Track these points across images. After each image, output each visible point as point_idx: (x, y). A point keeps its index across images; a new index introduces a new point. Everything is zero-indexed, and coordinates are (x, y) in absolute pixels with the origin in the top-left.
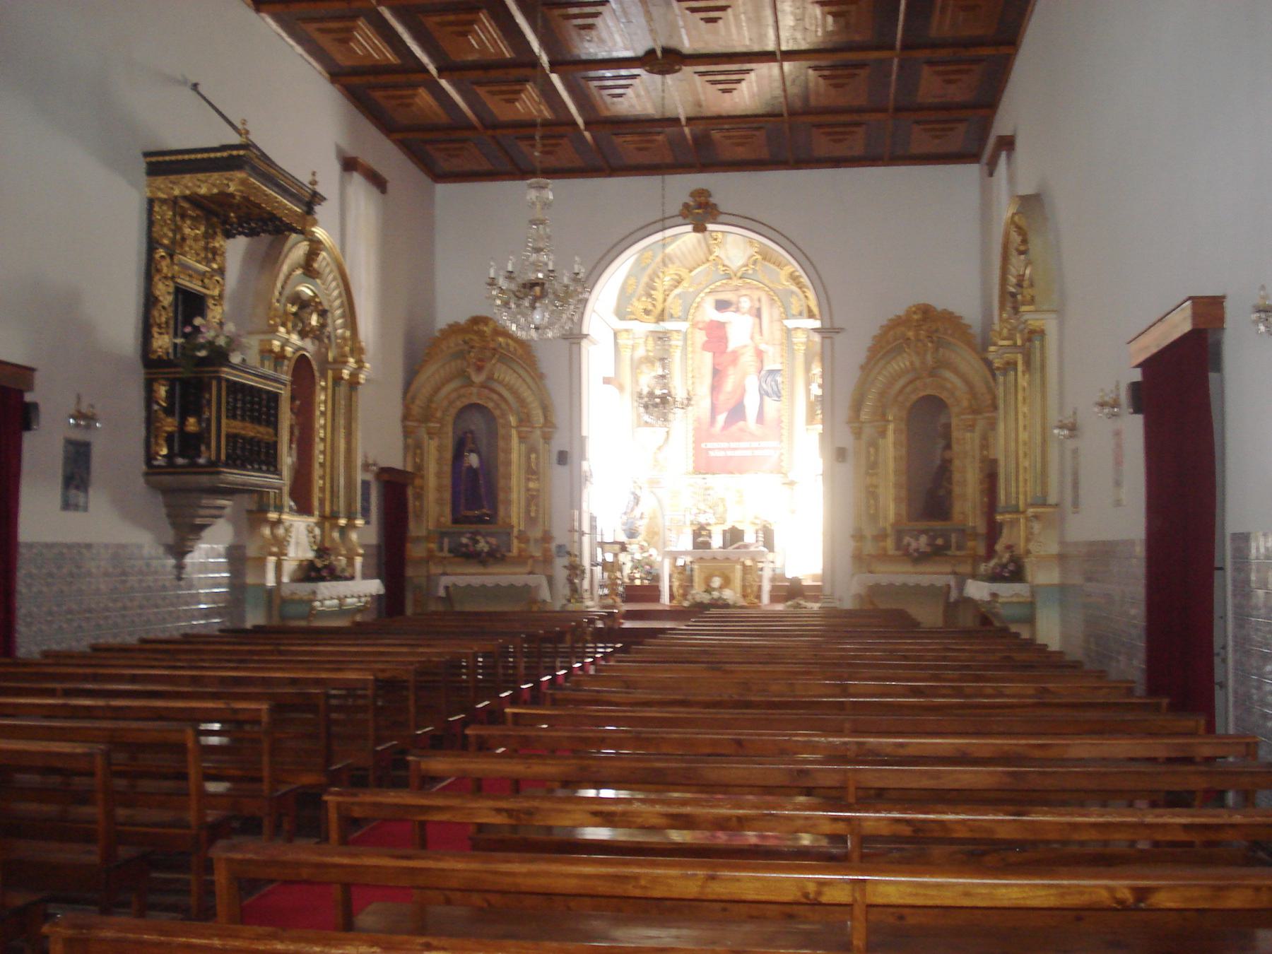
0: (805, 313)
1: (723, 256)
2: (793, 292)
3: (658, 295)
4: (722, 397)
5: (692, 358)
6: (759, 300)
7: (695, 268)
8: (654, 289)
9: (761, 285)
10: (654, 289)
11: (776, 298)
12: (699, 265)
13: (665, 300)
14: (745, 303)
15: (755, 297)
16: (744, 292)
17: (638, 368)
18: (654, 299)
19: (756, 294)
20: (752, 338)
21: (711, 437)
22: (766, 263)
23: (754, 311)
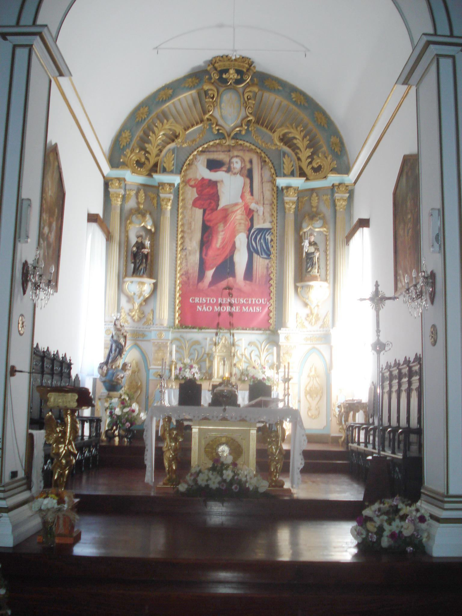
0: (297, 172)
1: (217, 113)
2: (284, 154)
3: (153, 149)
4: (211, 253)
6: (251, 162)
7: (188, 128)
8: (149, 142)
9: (254, 147)
10: (149, 142)
11: (267, 160)
12: (193, 126)
13: (158, 155)
14: (237, 165)
15: (247, 159)
16: (236, 153)
17: (127, 218)
18: (148, 152)
19: (247, 156)
20: (242, 197)
21: (198, 292)
22: (259, 127)
23: (245, 172)
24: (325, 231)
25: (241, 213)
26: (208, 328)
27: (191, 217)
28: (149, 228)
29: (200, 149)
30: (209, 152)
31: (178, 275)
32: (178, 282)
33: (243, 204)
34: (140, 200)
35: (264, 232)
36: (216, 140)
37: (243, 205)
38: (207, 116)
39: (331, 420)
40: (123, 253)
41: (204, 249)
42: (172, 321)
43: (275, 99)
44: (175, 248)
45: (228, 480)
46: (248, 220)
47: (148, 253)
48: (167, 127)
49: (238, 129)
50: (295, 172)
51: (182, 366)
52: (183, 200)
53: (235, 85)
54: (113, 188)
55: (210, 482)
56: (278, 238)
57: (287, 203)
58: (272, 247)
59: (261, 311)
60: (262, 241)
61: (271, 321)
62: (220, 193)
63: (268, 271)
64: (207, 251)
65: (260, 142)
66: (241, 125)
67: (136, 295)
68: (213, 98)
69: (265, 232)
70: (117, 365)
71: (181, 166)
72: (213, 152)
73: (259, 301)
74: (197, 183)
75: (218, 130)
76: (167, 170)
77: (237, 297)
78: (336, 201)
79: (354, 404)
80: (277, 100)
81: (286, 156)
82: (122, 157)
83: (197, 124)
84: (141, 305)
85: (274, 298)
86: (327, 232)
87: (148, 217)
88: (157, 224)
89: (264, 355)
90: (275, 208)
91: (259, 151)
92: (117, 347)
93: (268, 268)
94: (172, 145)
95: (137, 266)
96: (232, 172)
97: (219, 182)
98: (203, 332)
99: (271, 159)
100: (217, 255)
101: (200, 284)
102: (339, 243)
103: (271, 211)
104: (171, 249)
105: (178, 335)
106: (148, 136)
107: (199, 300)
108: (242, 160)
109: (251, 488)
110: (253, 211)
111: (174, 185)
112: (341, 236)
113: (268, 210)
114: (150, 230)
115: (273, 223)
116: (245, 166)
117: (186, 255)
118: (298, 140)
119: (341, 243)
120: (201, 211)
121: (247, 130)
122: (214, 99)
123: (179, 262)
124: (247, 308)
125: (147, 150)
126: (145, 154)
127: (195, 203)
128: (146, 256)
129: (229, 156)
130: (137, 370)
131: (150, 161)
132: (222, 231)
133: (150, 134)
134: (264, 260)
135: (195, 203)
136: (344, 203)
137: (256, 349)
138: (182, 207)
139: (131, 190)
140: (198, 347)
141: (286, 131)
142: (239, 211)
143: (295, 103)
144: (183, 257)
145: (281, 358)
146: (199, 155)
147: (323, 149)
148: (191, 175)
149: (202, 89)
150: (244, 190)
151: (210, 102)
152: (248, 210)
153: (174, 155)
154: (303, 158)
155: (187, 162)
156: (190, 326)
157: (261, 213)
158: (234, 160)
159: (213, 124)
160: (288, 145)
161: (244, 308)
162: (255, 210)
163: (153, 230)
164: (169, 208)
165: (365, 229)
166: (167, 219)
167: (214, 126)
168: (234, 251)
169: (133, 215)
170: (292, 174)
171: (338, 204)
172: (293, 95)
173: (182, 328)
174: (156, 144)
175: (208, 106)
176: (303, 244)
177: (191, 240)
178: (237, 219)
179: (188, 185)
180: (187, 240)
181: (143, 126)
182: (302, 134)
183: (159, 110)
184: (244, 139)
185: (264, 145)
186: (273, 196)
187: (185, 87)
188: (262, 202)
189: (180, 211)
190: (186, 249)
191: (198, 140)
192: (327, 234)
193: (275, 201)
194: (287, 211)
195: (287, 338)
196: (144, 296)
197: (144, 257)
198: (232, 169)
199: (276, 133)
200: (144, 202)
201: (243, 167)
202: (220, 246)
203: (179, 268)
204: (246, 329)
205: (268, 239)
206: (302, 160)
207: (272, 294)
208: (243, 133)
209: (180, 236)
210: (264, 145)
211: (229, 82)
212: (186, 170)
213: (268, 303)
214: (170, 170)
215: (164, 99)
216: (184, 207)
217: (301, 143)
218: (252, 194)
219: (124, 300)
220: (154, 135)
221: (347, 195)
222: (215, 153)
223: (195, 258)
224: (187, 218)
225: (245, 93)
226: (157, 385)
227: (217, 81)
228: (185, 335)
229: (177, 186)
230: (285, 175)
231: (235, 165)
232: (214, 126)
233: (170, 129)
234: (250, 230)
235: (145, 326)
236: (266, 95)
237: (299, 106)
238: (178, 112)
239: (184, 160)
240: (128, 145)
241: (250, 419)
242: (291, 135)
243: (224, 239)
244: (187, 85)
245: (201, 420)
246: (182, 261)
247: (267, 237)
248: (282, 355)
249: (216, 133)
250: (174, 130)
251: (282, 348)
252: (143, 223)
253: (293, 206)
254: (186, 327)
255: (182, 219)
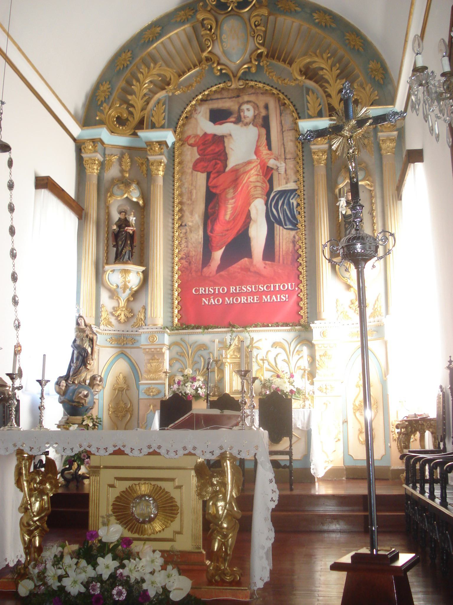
0: (326, 111)
1: (218, 51)
2: (308, 90)
3: (137, 102)
4: (218, 228)
5: (180, 179)
6: (266, 107)
7: (184, 73)
8: (132, 93)
9: (268, 88)
10: (132, 93)
11: (287, 101)
12: (189, 69)
13: (143, 109)
14: (249, 112)
15: (261, 104)
16: (246, 98)
17: (108, 191)
18: (133, 106)
19: (261, 101)
20: (257, 152)
21: (203, 280)
22: (274, 62)
23: (260, 121)
24: (368, 185)
25: (256, 173)
26: (217, 328)
27: (192, 185)
28: (135, 200)
29: (200, 97)
30: (212, 100)
31: (176, 259)
32: (176, 268)
33: (259, 161)
34: (123, 167)
35: (287, 194)
36: (220, 84)
37: (258, 162)
38: (205, 54)
39: (390, 447)
40: (103, 235)
41: (209, 223)
42: (170, 319)
43: (292, 24)
44: (171, 225)
45: (105, 577)
46: (266, 181)
47: (134, 232)
48: (155, 72)
49: (246, 66)
50: (323, 112)
51: (181, 378)
52: (179, 163)
53: (237, 10)
54: (86, 153)
55: (67, 582)
56: (306, 201)
57: (314, 153)
58: (299, 213)
59: (287, 300)
60: (285, 207)
61: (302, 313)
62: (228, 151)
63: (295, 246)
64: (213, 226)
65: (275, 78)
66: (249, 60)
67: (120, 287)
68: (210, 30)
69: (289, 194)
70: (82, 380)
71: (176, 120)
72: (218, 99)
73: (284, 286)
74: (198, 140)
75: (221, 70)
76: (156, 125)
77: (255, 283)
78: (381, 142)
79: (417, 421)
80: (295, 24)
81: (310, 93)
82: (99, 113)
83: (195, 66)
84: (128, 301)
85: (304, 282)
86: (371, 186)
87: (134, 186)
88: (146, 196)
89: (294, 359)
90: (301, 162)
91: (275, 91)
92: (79, 353)
93: (294, 242)
94: (161, 95)
95: (120, 249)
96: (243, 122)
97: (226, 136)
98: (210, 333)
99: (292, 100)
100: (228, 230)
101: (205, 269)
102: (388, 200)
103: (295, 167)
104: (165, 226)
105: (177, 338)
106: (131, 85)
107: (205, 291)
108: (256, 106)
109: (152, 593)
110: (272, 169)
111: (165, 143)
112: (390, 189)
113: (292, 166)
114: (137, 203)
115: (299, 183)
116: (259, 114)
117: (186, 233)
118: (324, 71)
119: (391, 199)
120: (204, 175)
121: (258, 67)
122: (213, 31)
123: (176, 242)
124: (269, 297)
125: (131, 102)
126: (127, 108)
127: (196, 167)
128: (132, 237)
129: (238, 102)
130: (125, 387)
131: (135, 116)
132: (232, 198)
133: (132, 82)
134: (288, 231)
135: (196, 167)
136: (392, 145)
137: (281, 351)
138: (178, 173)
139: (112, 155)
140: (204, 353)
141: (308, 60)
142: (253, 171)
143: (318, 25)
144: (182, 235)
145: (317, 362)
146: (200, 105)
147: (360, 79)
148: (189, 131)
149: (198, 20)
150: (259, 144)
151: (207, 34)
152: (266, 168)
153: (164, 106)
154: (333, 93)
155: (184, 115)
156: (193, 325)
157: (282, 171)
158: (245, 107)
159: (214, 63)
160: (314, 80)
161: (264, 297)
162: (275, 167)
163: (141, 202)
164: (161, 173)
165: (419, 166)
166: (159, 186)
167: (215, 65)
168: (249, 223)
169: (114, 185)
170: (320, 115)
171: (384, 146)
172: (316, 16)
173: (183, 329)
174: (142, 94)
175: (205, 41)
176: (338, 204)
177: (192, 213)
178: (251, 182)
179: (186, 144)
180: (187, 214)
181: (125, 75)
182: (330, 62)
183: (144, 54)
184: (256, 79)
185: (280, 82)
186: (297, 147)
187: (176, 21)
188: (283, 157)
189: (177, 176)
190: (186, 225)
191: (194, 84)
192: (372, 189)
193: (300, 154)
194: (315, 163)
195: (323, 334)
196: (131, 289)
197: (128, 236)
198: (243, 119)
199: (294, 65)
200: (130, 169)
201: (257, 114)
202: (230, 218)
203: (177, 251)
204: (268, 326)
205: (293, 203)
206: (332, 96)
207: (301, 276)
208: (253, 70)
209: (177, 209)
210: (280, 82)
211: (229, 7)
212: (184, 125)
213: (297, 289)
214: (160, 125)
215: (151, 39)
216: (182, 172)
217: (329, 75)
218: (270, 148)
219: (104, 295)
220: (138, 83)
221: (395, 133)
222: (220, 101)
223: (198, 236)
224: (186, 185)
225: (251, 18)
226: (150, 406)
227: (215, 9)
228: (186, 338)
229: (171, 147)
230: (310, 117)
231: (245, 114)
232: (215, 65)
233: (159, 75)
234: (268, 194)
235: (135, 329)
236: (281, 19)
237: (325, 27)
238: (169, 53)
239: (180, 113)
240: (107, 100)
241: (168, 451)
242: (315, 66)
243: (234, 209)
244: (179, 20)
245: (110, 454)
246: (181, 241)
247: (291, 201)
248: (318, 358)
249: (218, 74)
250: (164, 75)
251: (317, 348)
252: (125, 193)
253: (324, 156)
254: (187, 327)
255: (180, 187)
